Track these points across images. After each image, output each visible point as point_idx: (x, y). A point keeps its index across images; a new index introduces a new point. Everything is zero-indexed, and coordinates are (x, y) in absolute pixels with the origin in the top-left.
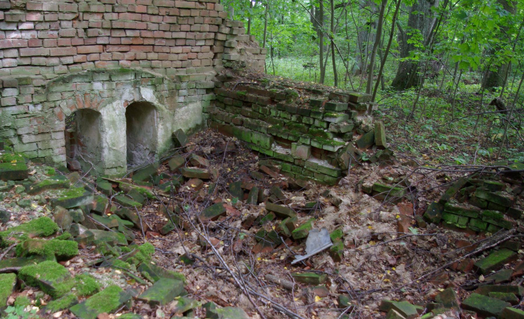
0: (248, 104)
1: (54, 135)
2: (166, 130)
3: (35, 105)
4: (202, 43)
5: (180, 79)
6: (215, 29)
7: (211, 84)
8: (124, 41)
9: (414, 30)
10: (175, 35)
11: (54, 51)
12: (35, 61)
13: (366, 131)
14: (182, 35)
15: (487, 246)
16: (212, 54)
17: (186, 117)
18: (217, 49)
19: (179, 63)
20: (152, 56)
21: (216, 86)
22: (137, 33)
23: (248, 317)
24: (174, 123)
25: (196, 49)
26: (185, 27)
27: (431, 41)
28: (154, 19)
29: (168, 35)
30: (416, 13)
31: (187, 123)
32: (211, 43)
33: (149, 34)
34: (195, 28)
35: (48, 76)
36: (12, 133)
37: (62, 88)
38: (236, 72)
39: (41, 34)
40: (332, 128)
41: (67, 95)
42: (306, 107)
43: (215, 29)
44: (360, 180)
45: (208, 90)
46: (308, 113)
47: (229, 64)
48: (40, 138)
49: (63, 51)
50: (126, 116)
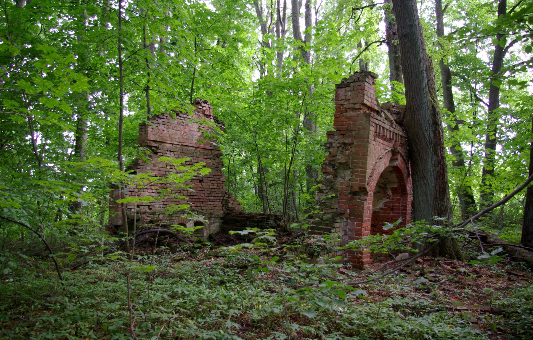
0: (238, 222)
2: (207, 233)
5: (211, 214)
6: (223, 195)
7: (222, 216)
8: (193, 200)
10: (210, 198)
13: (282, 226)
14: (212, 198)
15: (358, 319)
16: (222, 205)
17: (214, 228)
18: (224, 203)
19: (211, 208)
20: (202, 205)
21: (224, 217)
22: (197, 197)
24: (210, 230)
25: (216, 203)
26: (213, 195)
28: (203, 192)
29: (207, 198)
31: (214, 231)
32: (221, 201)
33: (201, 198)
34: (216, 195)
38: (232, 211)
40: (270, 225)
42: (260, 219)
43: (223, 195)
45: (221, 218)
46: (261, 222)
47: (228, 208)
50: (490, 95)
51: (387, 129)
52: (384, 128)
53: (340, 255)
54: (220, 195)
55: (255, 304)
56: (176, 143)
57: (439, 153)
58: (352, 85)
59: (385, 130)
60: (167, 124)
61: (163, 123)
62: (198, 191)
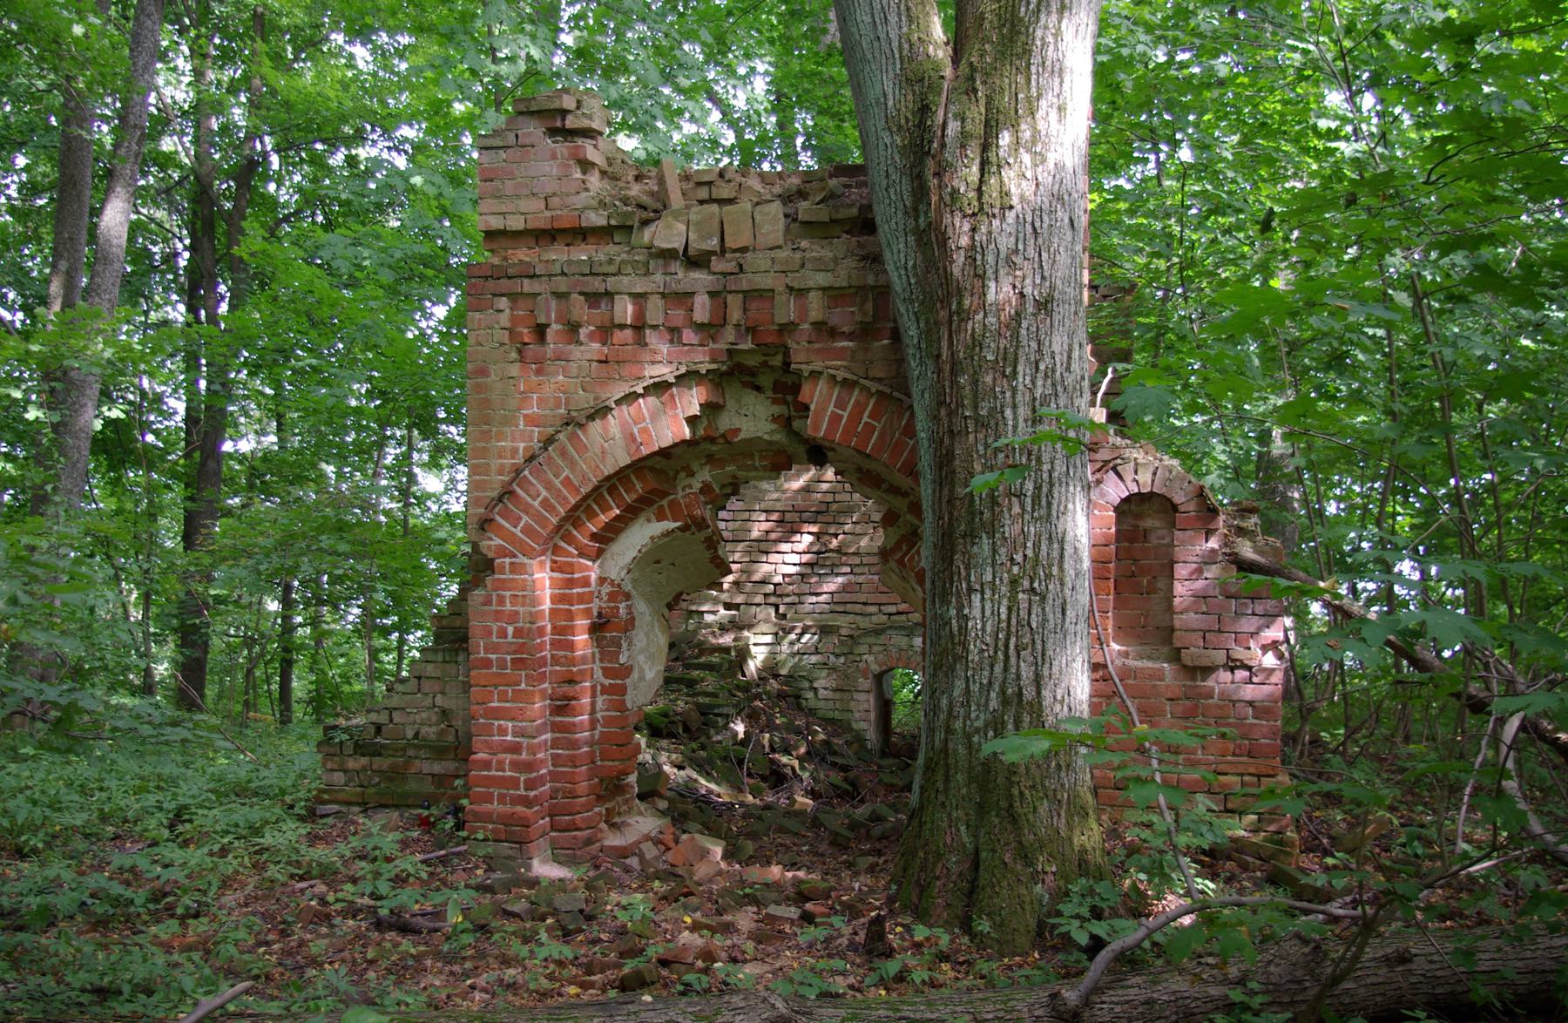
1: (855, 695)
3: (837, 656)
11: (871, 598)
12: (849, 607)
23: (1255, 1019)
27: (912, 332)
35: (862, 625)
36: (806, 684)
37: (872, 640)
39: (861, 579)
41: (875, 649)
48: (838, 695)
49: (883, 598)
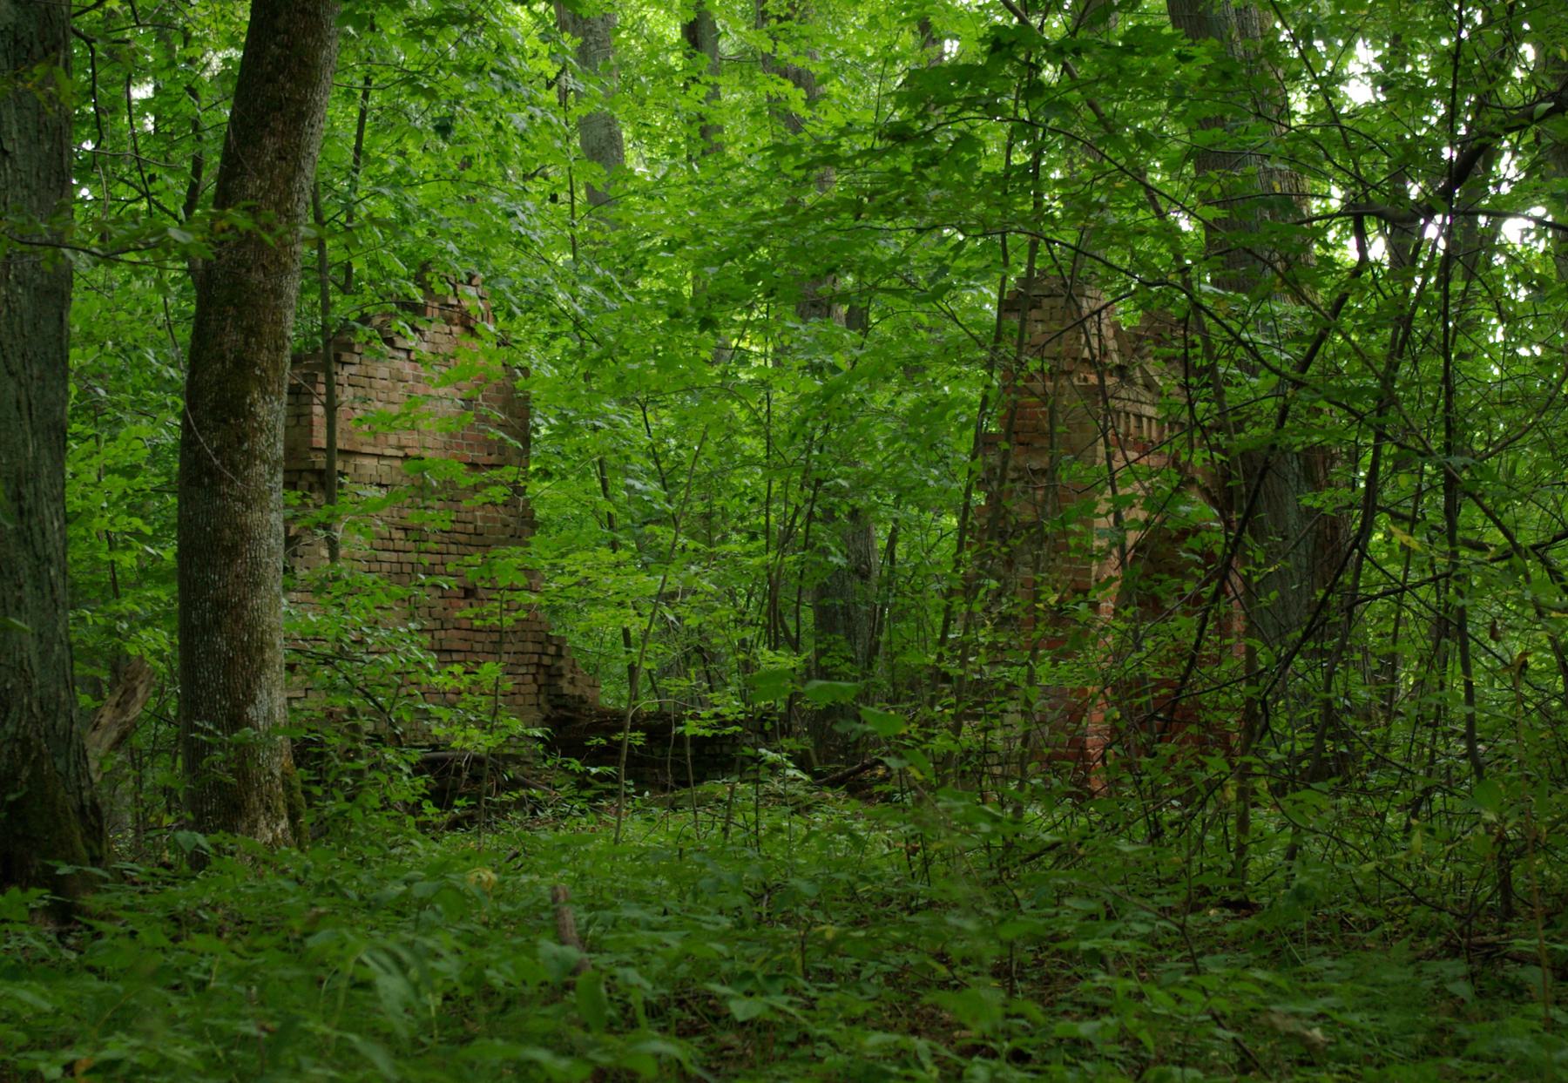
4: (522, 671)
6: (538, 648)
9: (830, 638)
16: (534, 688)
18: (541, 679)
28: (479, 636)
30: (827, 602)
32: (533, 670)
38: (576, 710)
43: (538, 648)
44: (326, 813)
51: (1150, 419)
52: (1139, 417)
53: (945, 924)
54: (530, 647)
55: (1308, 917)
56: (388, 452)
57: (1321, 474)
58: (1046, 301)
59: (1145, 420)
60: (364, 382)
61: (354, 380)
62: (463, 634)
